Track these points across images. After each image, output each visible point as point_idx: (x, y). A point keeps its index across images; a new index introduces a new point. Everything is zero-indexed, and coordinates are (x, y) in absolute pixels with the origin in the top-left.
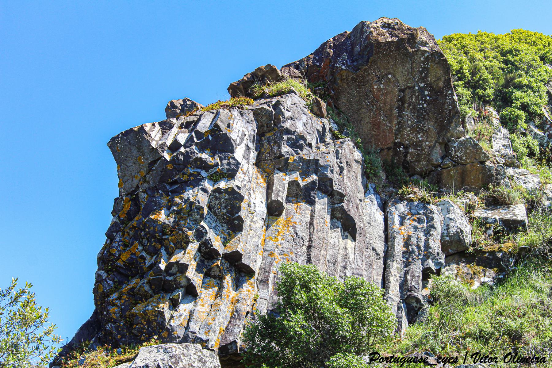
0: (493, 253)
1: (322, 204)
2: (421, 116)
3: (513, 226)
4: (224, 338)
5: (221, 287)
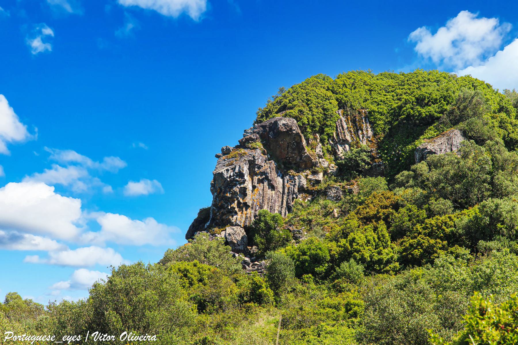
0: (311, 190)
1: (266, 183)
2: (294, 149)
3: (318, 182)
4: (244, 224)
5: (243, 211)
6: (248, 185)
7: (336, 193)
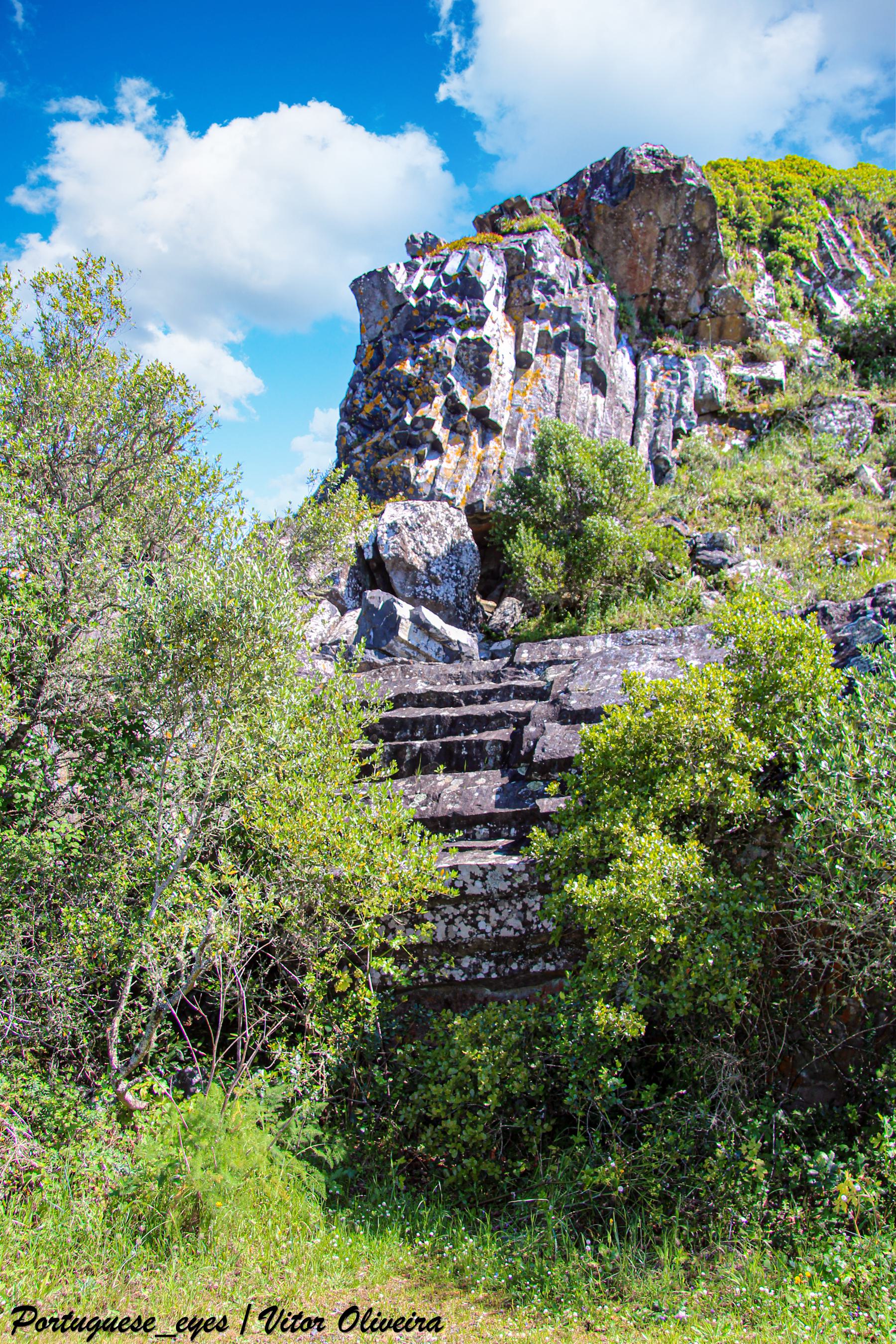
0: (746, 414)
1: (572, 356)
2: (682, 260)
3: (769, 386)
4: (470, 496)
5: (467, 444)
6: (497, 329)
7: (849, 420)
